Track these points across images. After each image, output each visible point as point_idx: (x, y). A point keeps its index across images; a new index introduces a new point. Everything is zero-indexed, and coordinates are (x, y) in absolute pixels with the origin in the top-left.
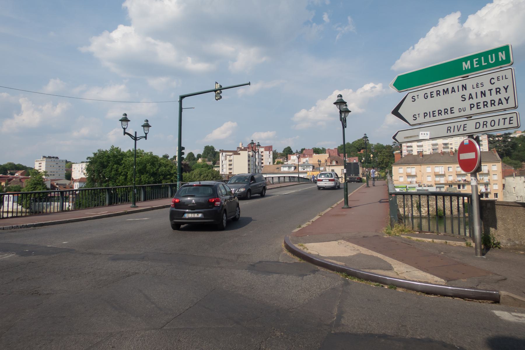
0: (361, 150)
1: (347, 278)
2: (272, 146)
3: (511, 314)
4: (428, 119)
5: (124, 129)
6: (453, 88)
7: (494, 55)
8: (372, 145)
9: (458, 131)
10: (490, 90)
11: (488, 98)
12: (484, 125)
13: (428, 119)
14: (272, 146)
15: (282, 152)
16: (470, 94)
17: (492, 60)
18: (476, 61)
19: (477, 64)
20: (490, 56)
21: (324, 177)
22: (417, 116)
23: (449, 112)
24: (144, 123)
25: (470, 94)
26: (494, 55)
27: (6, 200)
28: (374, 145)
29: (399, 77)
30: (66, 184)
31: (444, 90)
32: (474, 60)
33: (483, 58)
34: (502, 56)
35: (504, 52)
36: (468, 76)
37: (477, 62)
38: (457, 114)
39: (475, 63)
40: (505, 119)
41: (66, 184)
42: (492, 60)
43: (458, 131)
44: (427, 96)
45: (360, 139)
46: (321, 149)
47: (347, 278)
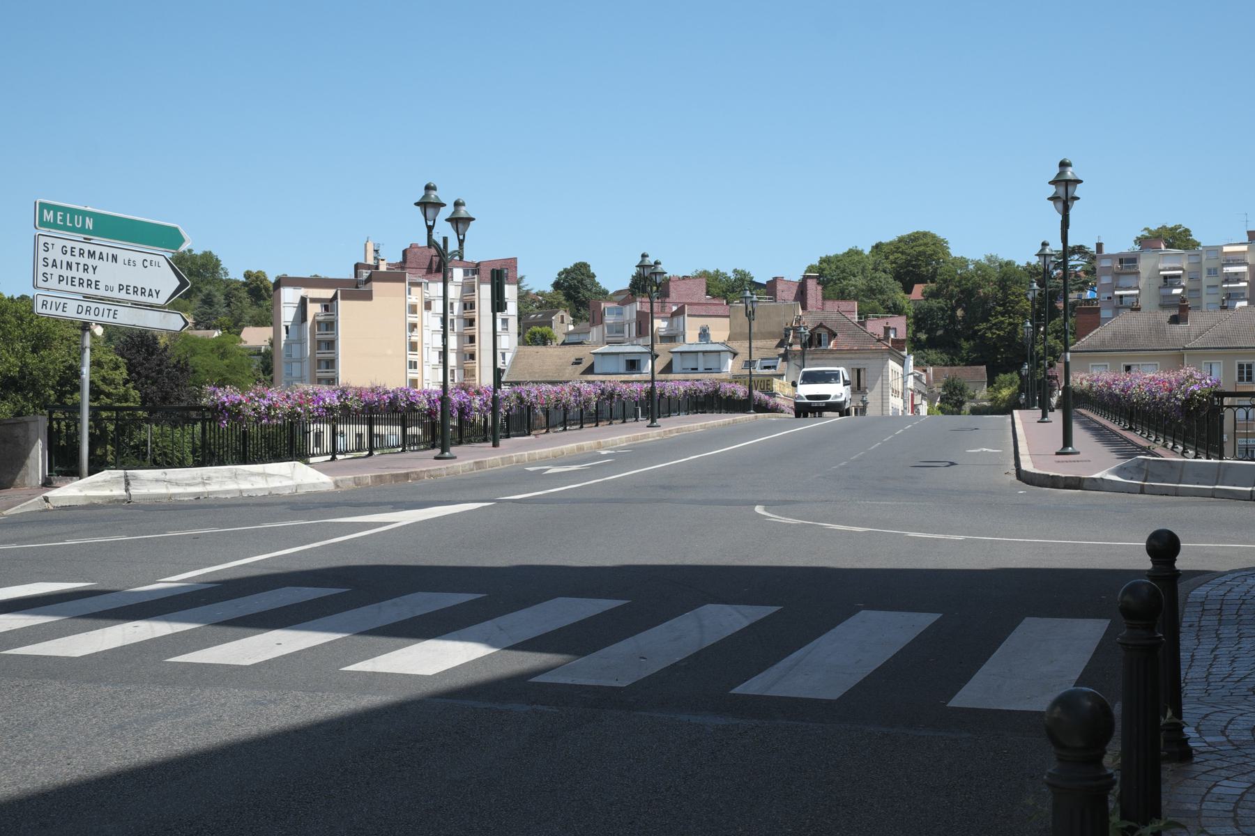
0: (916, 286)
1: (533, 316)
2: (516, 258)
3: (307, 463)
4: (123, 295)
5: (430, 229)
6: (101, 253)
7: (81, 217)
8: (963, 262)
9: (57, 310)
10: (78, 264)
11: (73, 273)
12: (87, 310)
13: (63, 286)
14: (516, 258)
15: (549, 289)
16: (54, 260)
17: (78, 224)
18: (61, 215)
19: (61, 220)
20: (76, 216)
21: (1078, 260)
22: (49, 276)
23: (93, 285)
24: (419, 194)
25: (54, 260)
26: (81, 217)
27: (85, 239)
28: (971, 267)
29: (176, 229)
30: (669, 297)
31: (89, 251)
32: (59, 213)
33: (68, 215)
34: (48, 216)
35: (52, 212)
36: (90, 239)
37: (61, 218)
38: (101, 292)
39: (59, 218)
40: (109, 310)
41: (669, 297)
42: (78, 224)
43: (57, 310)
44: (66, 251)
45: (909, 236)
46: (732, 276)
47: (533, 316)
